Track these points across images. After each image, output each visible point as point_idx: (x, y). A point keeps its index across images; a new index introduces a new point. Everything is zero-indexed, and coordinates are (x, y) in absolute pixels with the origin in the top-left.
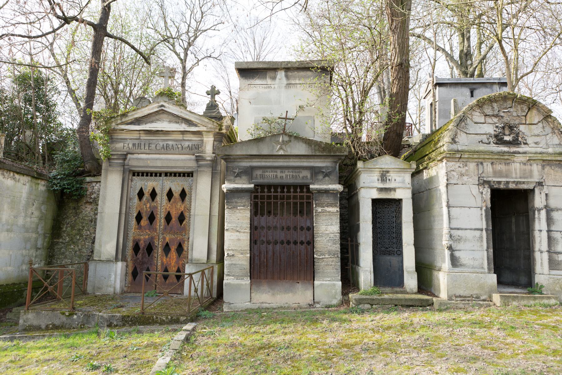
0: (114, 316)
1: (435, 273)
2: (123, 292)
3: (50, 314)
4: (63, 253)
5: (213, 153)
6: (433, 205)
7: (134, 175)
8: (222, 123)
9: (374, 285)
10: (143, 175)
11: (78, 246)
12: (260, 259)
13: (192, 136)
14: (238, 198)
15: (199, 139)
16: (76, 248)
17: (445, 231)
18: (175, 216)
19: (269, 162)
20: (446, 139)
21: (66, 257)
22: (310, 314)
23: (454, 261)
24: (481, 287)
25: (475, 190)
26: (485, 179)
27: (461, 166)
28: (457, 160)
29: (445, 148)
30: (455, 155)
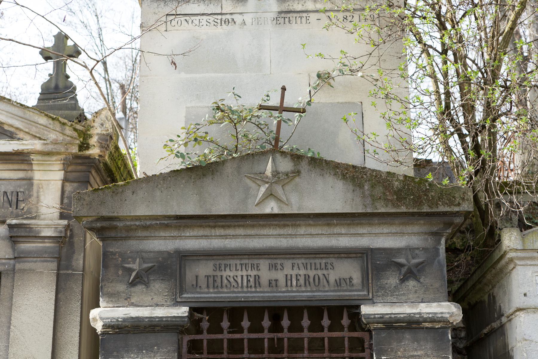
15: (21, 175)
19: (235, 236)
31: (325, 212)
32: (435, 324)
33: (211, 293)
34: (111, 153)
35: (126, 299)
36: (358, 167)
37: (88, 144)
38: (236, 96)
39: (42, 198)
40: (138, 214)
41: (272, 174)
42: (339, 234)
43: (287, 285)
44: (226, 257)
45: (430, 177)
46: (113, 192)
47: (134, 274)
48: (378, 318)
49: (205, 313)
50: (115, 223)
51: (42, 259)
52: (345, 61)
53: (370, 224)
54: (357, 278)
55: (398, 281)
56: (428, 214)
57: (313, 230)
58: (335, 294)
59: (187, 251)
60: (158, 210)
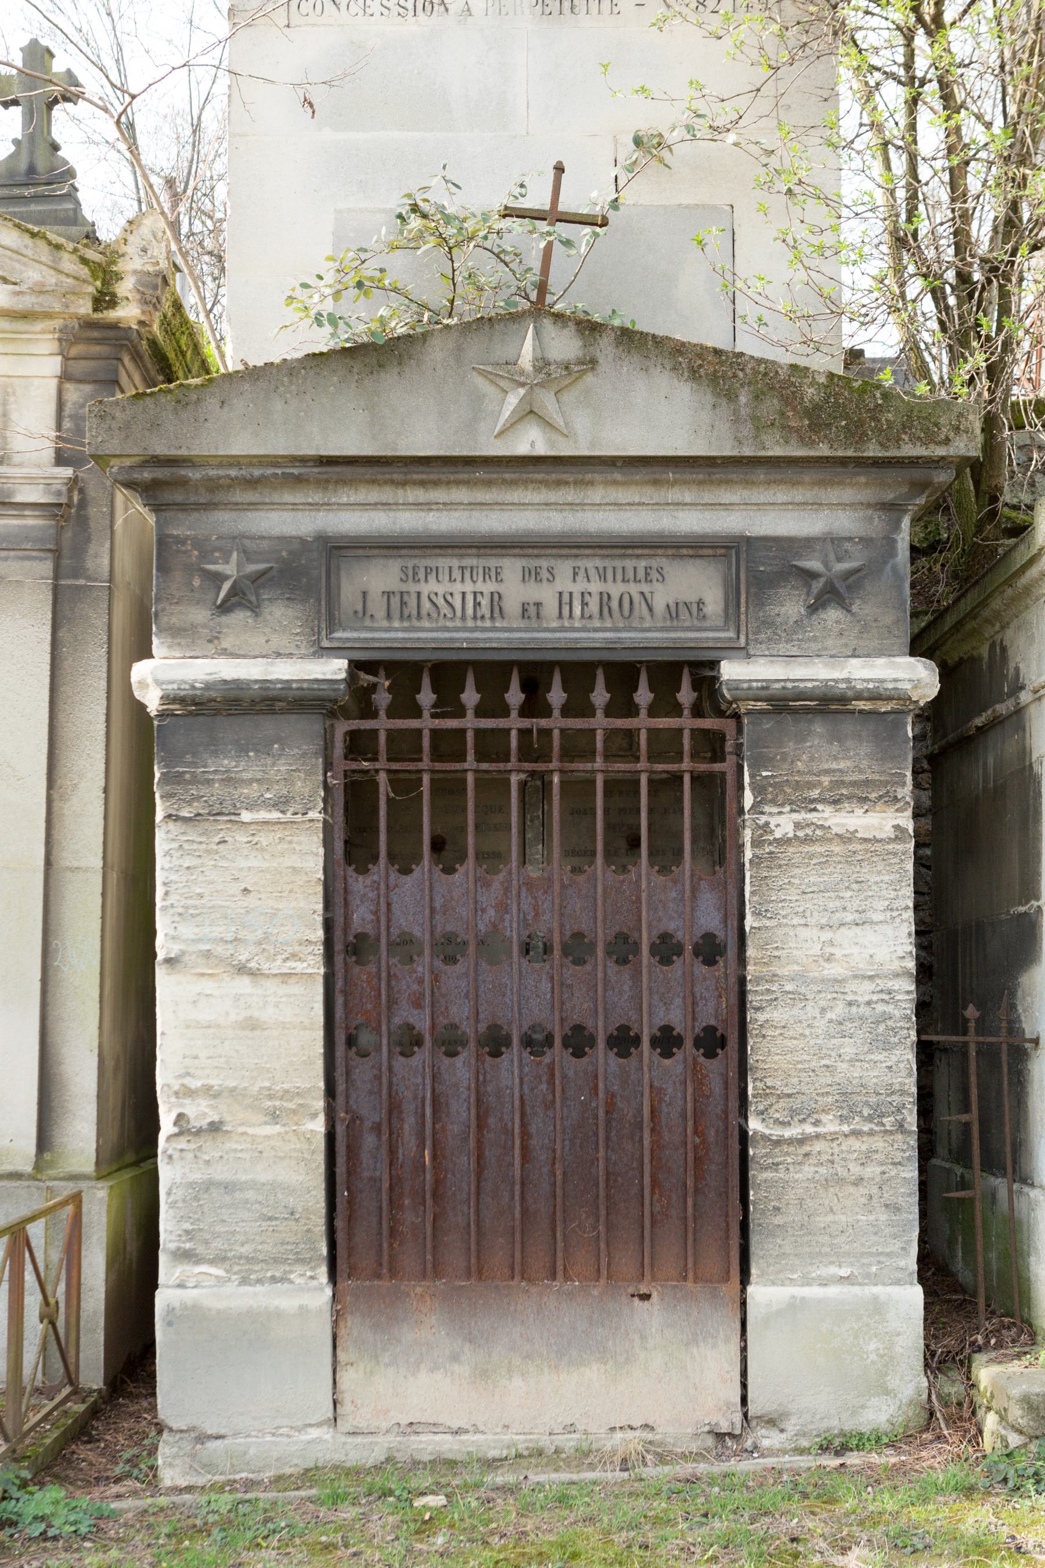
5: (61, 459)
12: (392, 1151)
14: (242, 750)
19: (449, 506)
31: (649, 454)
32: (880, 703)
33: (397, 630)
34: (165, 317)
35: (210, 641)
36: (727, 352)
37: (114, 295)
38: (450, 185)
39: (14, 416)
40: (233, 453)
41: (534, 366)
42: (678, 504)
43: (560, 616)
44: (429, 551)
45: (888, 376)
46: (178, 402)
47: (226, 586)
48: (758, 689)
49: (382, 673)
50: (183, 472)
51: (20, 553)
52: (701, 106)
53: (747, 483)
54: (714, 601)
55: (802, 610)
57: (620, 495)
58: (666, 635)
59: (342, 537)
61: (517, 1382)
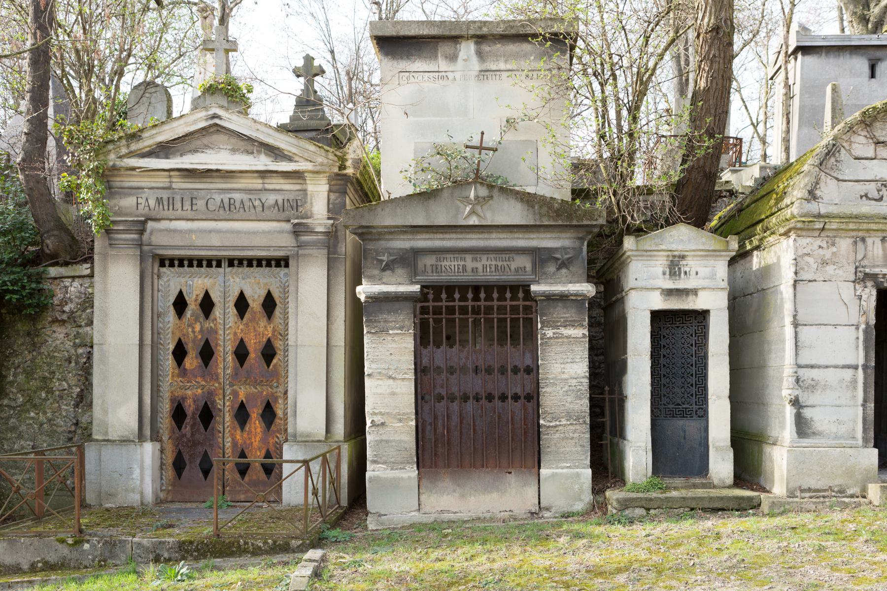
0: (164, 543)
1: (767, 449)
2: (159, 502)
3: (36, 543)
4: (14, 429)
6: (769, 321)
7: (162, 265)
8: (345, 154)
9: (653, 473)
10: (181, 265)
11: (45, 413)
12: (435, 431)
13: (282, 181)
14: (389, 312)
15: (298, 187)
16: (42, 418)
17: (788, 371)
18: (254, 347)
20: (796, 190)
21: (20, 436)
22: (535, 527)
23: (802, 427)
24: (849, 473)
25: (848, 291)
26: (867, 270)
27: (824, 245)
28: (817, 233)
29: (795, 210)
30: (815, 225)
39: (314, 204)
54: (529, 267)
56: (576, 226)
60: (399, 222)
61: (473, 498)
